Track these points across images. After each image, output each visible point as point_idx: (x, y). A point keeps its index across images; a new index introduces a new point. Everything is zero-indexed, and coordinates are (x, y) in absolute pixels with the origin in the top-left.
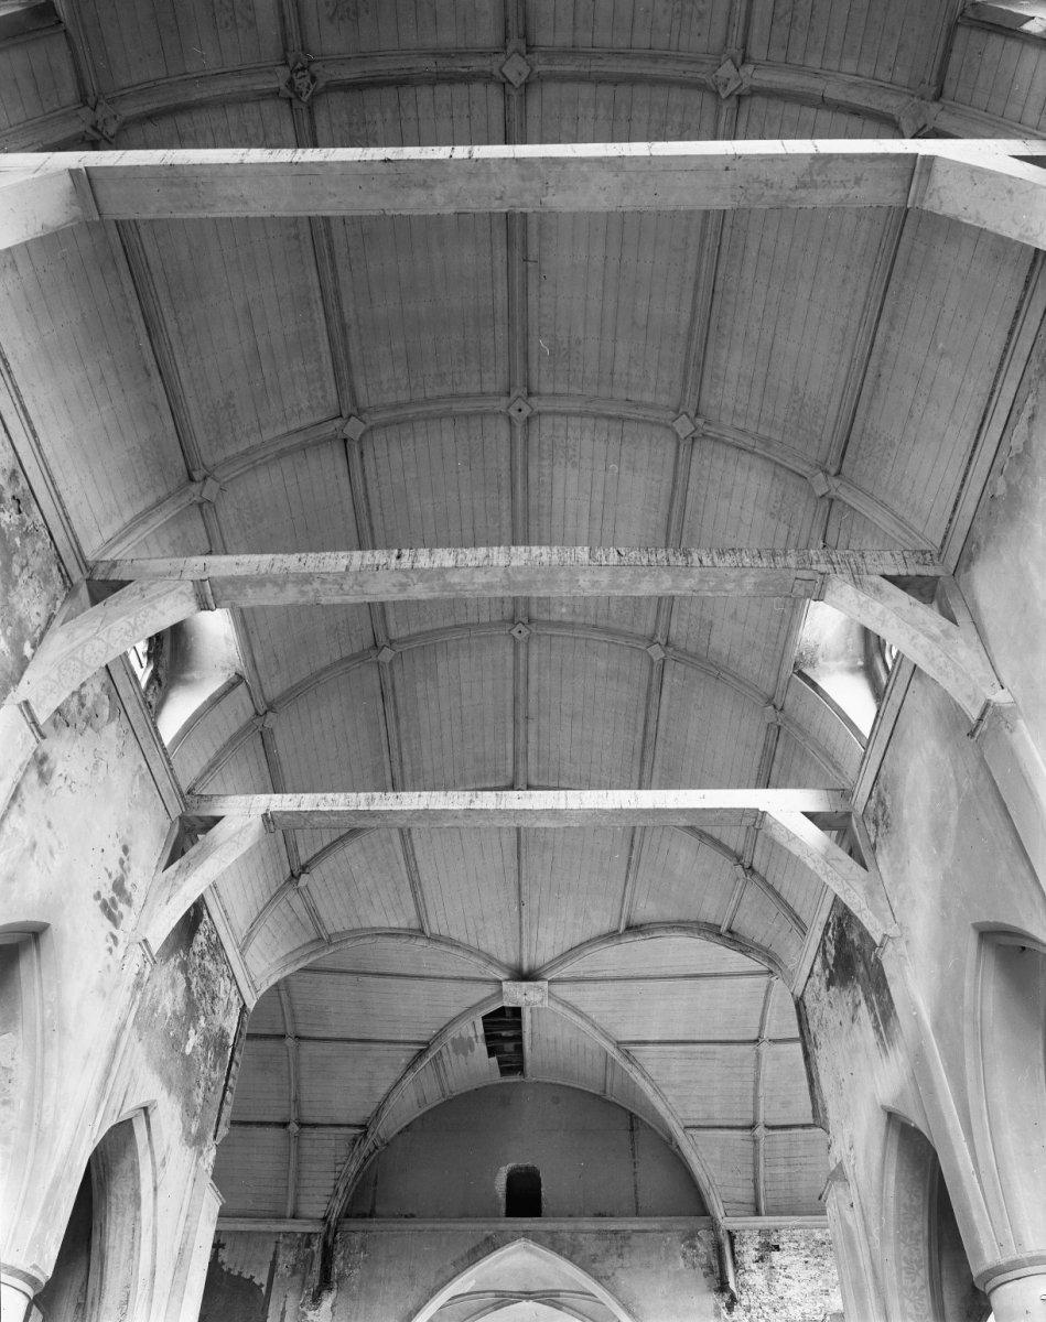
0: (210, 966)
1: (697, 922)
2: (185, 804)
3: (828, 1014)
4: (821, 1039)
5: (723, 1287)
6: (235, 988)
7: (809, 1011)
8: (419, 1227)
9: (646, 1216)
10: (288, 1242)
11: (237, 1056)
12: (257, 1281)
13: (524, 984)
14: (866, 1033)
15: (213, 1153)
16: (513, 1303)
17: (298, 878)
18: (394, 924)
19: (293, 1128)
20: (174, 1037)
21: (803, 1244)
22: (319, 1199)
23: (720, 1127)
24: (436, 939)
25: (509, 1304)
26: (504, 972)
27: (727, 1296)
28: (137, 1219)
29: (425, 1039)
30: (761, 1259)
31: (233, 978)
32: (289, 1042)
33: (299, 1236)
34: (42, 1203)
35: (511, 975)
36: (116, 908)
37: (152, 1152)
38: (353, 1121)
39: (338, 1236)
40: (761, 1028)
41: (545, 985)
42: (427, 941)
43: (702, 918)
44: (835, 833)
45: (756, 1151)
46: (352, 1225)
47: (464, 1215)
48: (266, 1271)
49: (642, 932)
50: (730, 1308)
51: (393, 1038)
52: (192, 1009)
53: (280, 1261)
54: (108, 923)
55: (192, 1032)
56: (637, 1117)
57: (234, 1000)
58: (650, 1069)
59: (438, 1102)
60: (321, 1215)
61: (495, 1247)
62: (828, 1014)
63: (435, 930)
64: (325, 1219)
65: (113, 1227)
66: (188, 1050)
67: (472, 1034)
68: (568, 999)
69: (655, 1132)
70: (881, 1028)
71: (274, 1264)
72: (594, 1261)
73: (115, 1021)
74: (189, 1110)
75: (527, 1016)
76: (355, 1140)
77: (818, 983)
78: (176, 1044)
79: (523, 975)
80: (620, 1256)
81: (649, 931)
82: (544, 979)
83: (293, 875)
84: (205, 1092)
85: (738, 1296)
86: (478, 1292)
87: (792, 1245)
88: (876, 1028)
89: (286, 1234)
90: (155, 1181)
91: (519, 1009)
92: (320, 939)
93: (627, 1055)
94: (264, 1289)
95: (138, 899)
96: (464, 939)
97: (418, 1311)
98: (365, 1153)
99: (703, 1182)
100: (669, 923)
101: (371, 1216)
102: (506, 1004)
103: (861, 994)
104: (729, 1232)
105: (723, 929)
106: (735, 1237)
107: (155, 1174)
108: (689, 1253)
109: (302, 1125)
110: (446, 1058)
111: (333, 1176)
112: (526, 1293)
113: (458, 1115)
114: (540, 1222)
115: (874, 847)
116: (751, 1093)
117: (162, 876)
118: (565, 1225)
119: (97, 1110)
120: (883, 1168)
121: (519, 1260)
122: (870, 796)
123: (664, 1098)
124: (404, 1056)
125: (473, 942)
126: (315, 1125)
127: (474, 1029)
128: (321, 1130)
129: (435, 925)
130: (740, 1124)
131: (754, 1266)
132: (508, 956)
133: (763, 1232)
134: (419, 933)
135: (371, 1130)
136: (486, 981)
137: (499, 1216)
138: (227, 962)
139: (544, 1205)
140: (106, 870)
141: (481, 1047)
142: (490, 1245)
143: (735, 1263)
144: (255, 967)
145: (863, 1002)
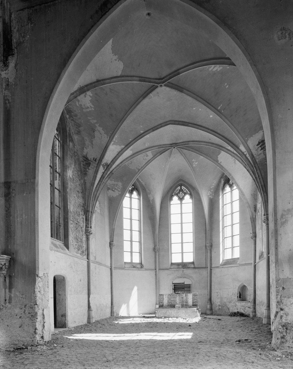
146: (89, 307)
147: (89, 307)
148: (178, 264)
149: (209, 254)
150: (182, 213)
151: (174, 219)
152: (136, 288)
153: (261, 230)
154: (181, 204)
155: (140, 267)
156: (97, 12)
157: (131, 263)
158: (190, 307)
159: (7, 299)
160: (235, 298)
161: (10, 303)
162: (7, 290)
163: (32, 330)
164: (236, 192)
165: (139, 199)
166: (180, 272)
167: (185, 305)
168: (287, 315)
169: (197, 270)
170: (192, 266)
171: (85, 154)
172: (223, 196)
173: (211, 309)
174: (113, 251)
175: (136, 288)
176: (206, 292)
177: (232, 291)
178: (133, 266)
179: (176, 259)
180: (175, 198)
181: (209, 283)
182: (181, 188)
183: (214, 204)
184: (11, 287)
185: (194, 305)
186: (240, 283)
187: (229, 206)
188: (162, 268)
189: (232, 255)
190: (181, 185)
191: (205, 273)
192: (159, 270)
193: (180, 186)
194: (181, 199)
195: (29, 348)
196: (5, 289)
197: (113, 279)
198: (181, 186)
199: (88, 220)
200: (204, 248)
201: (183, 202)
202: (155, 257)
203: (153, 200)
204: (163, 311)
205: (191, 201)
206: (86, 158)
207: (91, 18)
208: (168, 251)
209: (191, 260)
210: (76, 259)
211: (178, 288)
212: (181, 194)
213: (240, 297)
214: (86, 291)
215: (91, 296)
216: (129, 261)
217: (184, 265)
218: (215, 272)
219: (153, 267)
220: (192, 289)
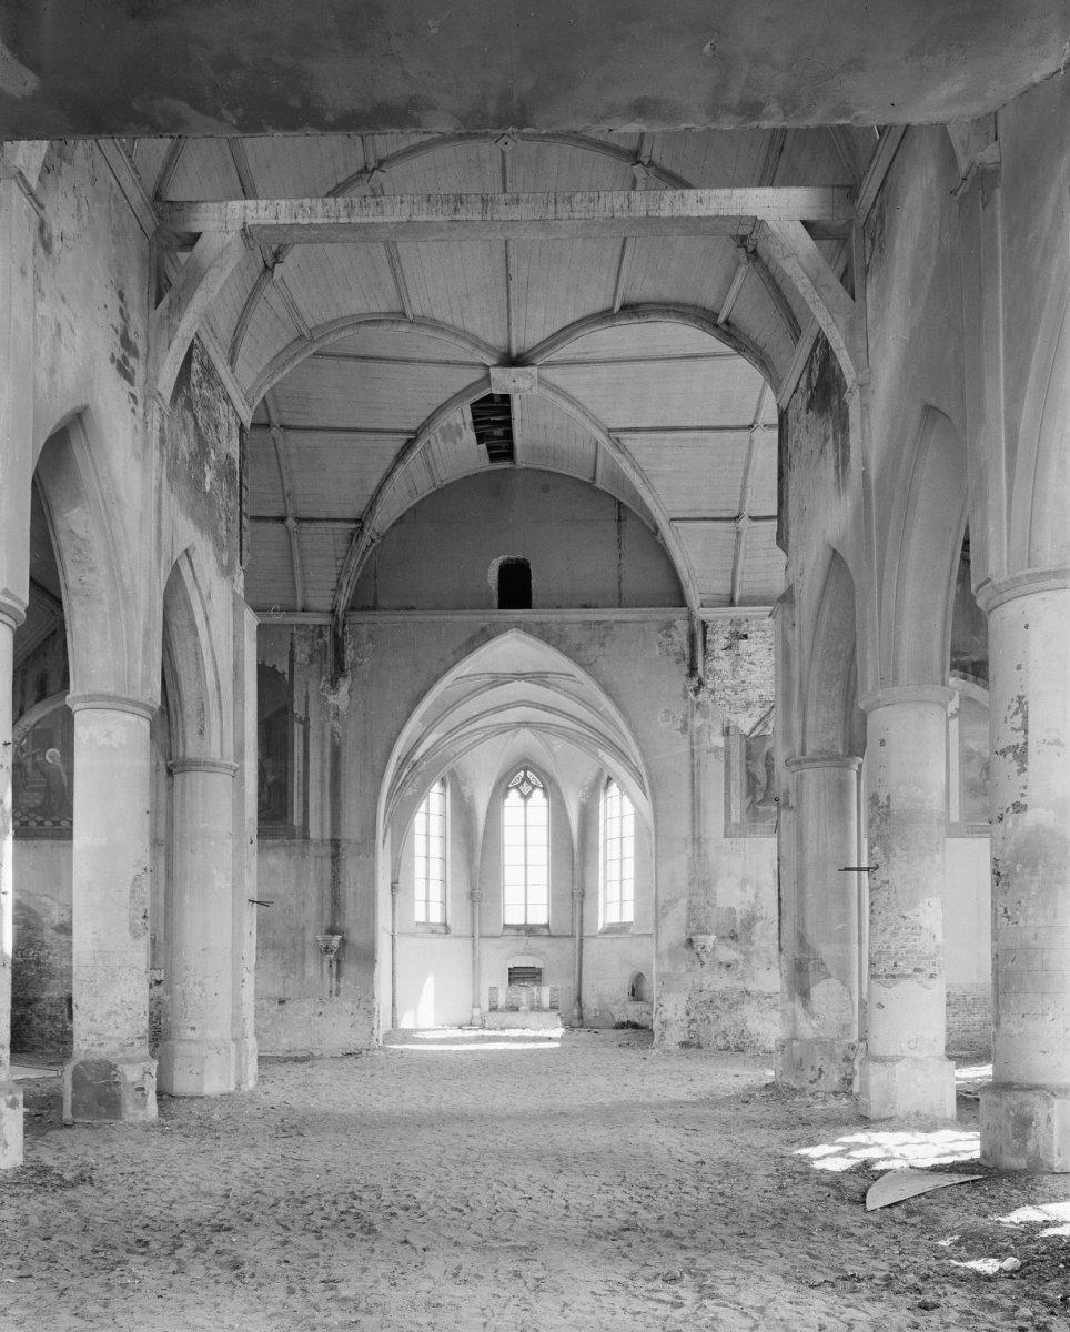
0: (207, 393)
1: (694, 307)
2: (159, 217)
3: (804, 438)
4: (795, 462)
5: (693, 670)
6: (231, 408)
7: (790, 428)
8: (420, 618)
9: (627, 607)
10: (302, 633)
11: (245, 480)
12: (279, 669)
13: (513, 370)
14: (829, 473)
15: (242, 577)
16: (507, 683)
17: (272, 269)
18: (374, 309)
19: (291, 522)
20: (195, 479)
21: (769, 634)
22: (322, 590)
23: (705, 519)
24: (420, 322)
25: (502, 684)
26: (491, 355)
27: (695, 679)
28: (197, 645)
29: (414, 427)
30: (729, 647)
31: (228, 399)
32: (275, 432)
33: (311, 628)
34: (141, 649)
35: (501, 359)
36: (128, 364)
37: (199, 588)
38: (348, 516)
39: (347, 628)
40: (757, 413)
41: (533, 370)
42: (409, 326)
43: (701, 302)
44: (835, 242)
45: (738, 542)
46: (357, 617)
47: (460, 607)
48: (286, 659)
49: (637, 314)
50: (696, 691)
51: (379, 426)
52: (202, 444)
53: (297, 650)
54: (126, 383)
55: (207, 468)
56: (625, 507)
57: (232, 420)
58: (640, 458)
59: (430, 491)
60: (329, 608)
61: (489, 638)
62: (804, 438)
63: (418, 312)
64: (333, 612)
65: (178, 650)
66: (208, 488)
67: (460, 421)
68: (557, 383)
69: (642, 522)
70: (840, 470)
71: (292, 653)
72: (578, 649)
73: (155, 483)
74: (219, 546)
75: (516, 403)
76: (352, 535)
77: (801, 402)
78: (197, 484)
79: (512, 360)
80: (602, 644)
81: (646, 313)
82: (534, 364)
83: (266, 266)
84: (226, 523)
85: (705, 680)
86: (475, 675)
87: (760, 634)
88: (837, 468)
89: (300, 626)
90: (205, 613)
91: (508, 396)
92: (301, 337)
93: (617, 444)
94: (287, 677)
95: (141, 348)
96: (448, 320)
97: (424, 694)
98: (363, 548)
99: (684, 575)
100: (666, 304)
101: (375, 609)
102: (494, 392)
103: (831, 428)
104: (703, 623)
105: (721, 319)
106: (707, 627)
107: (204, 607)
108: (666, 641)
109: (299, 520)
110: (434, 447)
111: (334, 570)
112: (517, 674)
113: (443, 506)
114: (529, 613)
115: (866, 270)
116: (740, 482)
117: (156, 314)
118: (552, 616)
119: (160, 568)
120: (822, 597)
121: (512, 648)
122: (874, 205)
123: (652, 489)
124: (393, 445)
125: (458, 322)
126: (312, 520)
127: (462, 416)
128: (318, 525)
129: (416, 307)
130: (725, 515)
131: (722, 654)
132: (496, 339)
133: (736, 622)
134: (399, 316)
135: (367, 525)
136: (472, 365)
137: (492, 608)
138: (220, 383)
139: (534, 597)
140: (113, 326)
141: (469, 435)
142: (485, 635)
143: (705, 650)
144: (241, 388)
145: (831, 438)
148: (518, 928)
149: (578, 910)
150: (525, 826)
151: (511, 836)
152: (430, 980)
154: (525, 806)
155: (443, 931)
156: (460, 648)
157: (426, 923)
158: (546, 1011)
160: (625, 995)
161: (337, 995)
162: (334, 979)
163: (368, 1030)
165: (444, 794)
166: (524, 942)
167: (536, 1008)
168: (666, 1011)
169: (554, 941)
170: (546, 932)
172: (606, 801)
173: (581, 1017)
174: (397, 900)
175: (430, 980)
176: (572, 983)
177: (619, 983)
178: (431, 929)
179: (514, 916)
180: (514, 794)
182: (525, 774)
183: (588, 814)
184: (339, 974)
185: (553, 1008)
186: (634, 969)
187: (616, 821)
188: (486, 933)
189: (621, 918)
190: (526, 770)
191: (570, 945)
192: (480, 937)
193: (522, 772)
194: (526, 797)
195: (364, 1052)
196: (331, 977)
197: (397, 957)
198: (526, 770)
200: (568, 898)
201: (530, 802)
202: (473, 912)
203: (472, 798)
204: (497, 1017)
205: (544, 802)
207: (454, 653)
208: (497, 897)
209: (543, 920)
211: (518, 975)
212: (526, 788)
213: (633, 994)
216: (424, 920)
217: (529, 930)
218: (592, 947)
219: (468, 933)
220: (545, 976)
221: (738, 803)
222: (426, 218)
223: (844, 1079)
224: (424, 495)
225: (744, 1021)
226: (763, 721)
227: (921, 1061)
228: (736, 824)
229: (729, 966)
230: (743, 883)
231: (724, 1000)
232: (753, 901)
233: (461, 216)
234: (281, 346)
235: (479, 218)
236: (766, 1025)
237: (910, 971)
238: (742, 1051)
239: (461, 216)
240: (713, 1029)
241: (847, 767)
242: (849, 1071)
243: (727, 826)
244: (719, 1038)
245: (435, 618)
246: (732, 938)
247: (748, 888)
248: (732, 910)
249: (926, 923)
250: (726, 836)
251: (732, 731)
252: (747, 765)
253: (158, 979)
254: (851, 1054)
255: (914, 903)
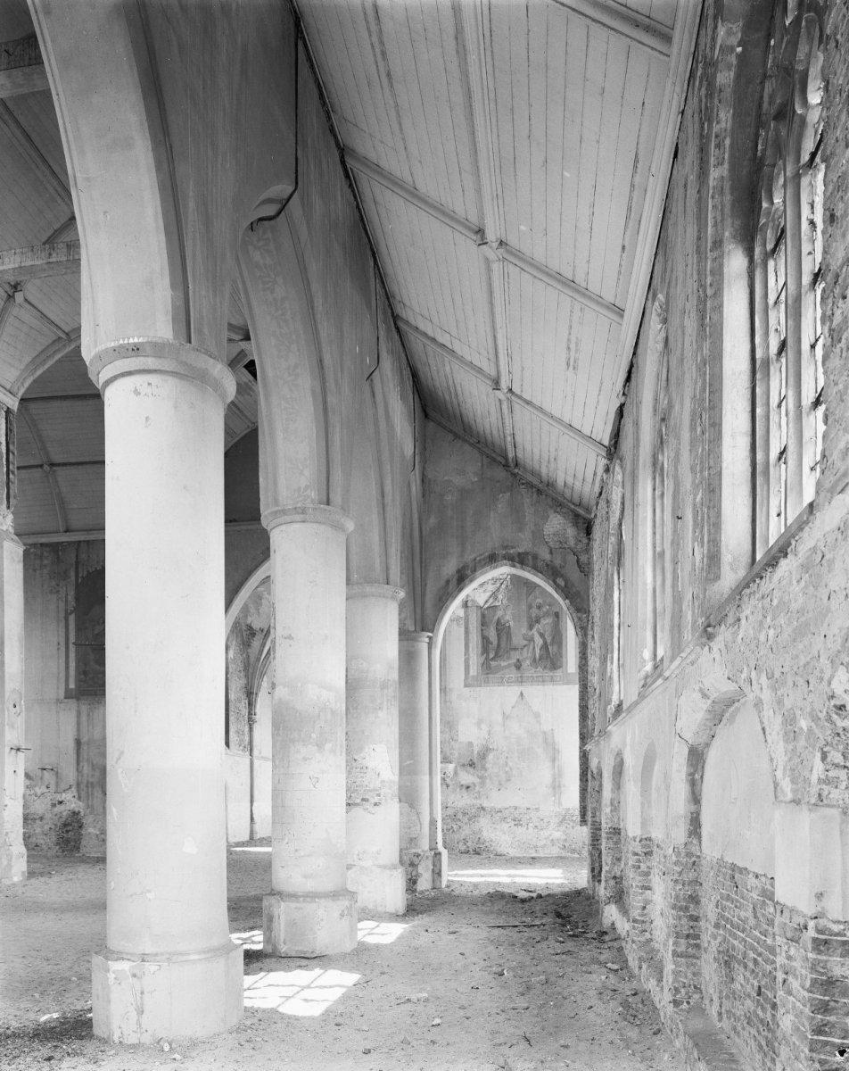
59: (245, 432)
146: (252, 819)
147: (252, 819)
153: (8, 387)
159: (587, 292)
164: (613, 746)
171: (249, 622)
181: (190, 278)
199: (251, 705)
206: (250, 628)
210: (237, 759)
214: (249, 798)
215: (255, 804)
221: (475, 660)
222: (32, 263)
223: (410, 880)
224: (241, 436)
225: (480, 831)
226: (494, 595)
227: (366, 869)
228: (473, 676)
229: (468, 787)
230: (479, 723)
231: (465, 814)
232: (487, 737)
233: (53, 259)
234: (40, 349)
235: (65, 259)
236: (498, 833)
237: (358, 801)
238: (479, 854)
239: (53, 259)
240: (456, 836)
241: (415, 640)
242: (414, 874)
243: (466, 678)
244: (461, 844)
245: (249, 527)
246: (471, 765)
247: (483, 726)
248: (470, 744)
249: (370, 763)
250: (466, 686)
251: (469, 604)
252: (482, 630)
253: (60, 800)
254: (416, 860)
255: (361, 749)
